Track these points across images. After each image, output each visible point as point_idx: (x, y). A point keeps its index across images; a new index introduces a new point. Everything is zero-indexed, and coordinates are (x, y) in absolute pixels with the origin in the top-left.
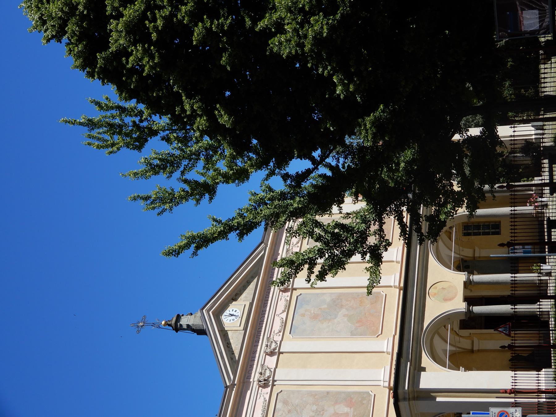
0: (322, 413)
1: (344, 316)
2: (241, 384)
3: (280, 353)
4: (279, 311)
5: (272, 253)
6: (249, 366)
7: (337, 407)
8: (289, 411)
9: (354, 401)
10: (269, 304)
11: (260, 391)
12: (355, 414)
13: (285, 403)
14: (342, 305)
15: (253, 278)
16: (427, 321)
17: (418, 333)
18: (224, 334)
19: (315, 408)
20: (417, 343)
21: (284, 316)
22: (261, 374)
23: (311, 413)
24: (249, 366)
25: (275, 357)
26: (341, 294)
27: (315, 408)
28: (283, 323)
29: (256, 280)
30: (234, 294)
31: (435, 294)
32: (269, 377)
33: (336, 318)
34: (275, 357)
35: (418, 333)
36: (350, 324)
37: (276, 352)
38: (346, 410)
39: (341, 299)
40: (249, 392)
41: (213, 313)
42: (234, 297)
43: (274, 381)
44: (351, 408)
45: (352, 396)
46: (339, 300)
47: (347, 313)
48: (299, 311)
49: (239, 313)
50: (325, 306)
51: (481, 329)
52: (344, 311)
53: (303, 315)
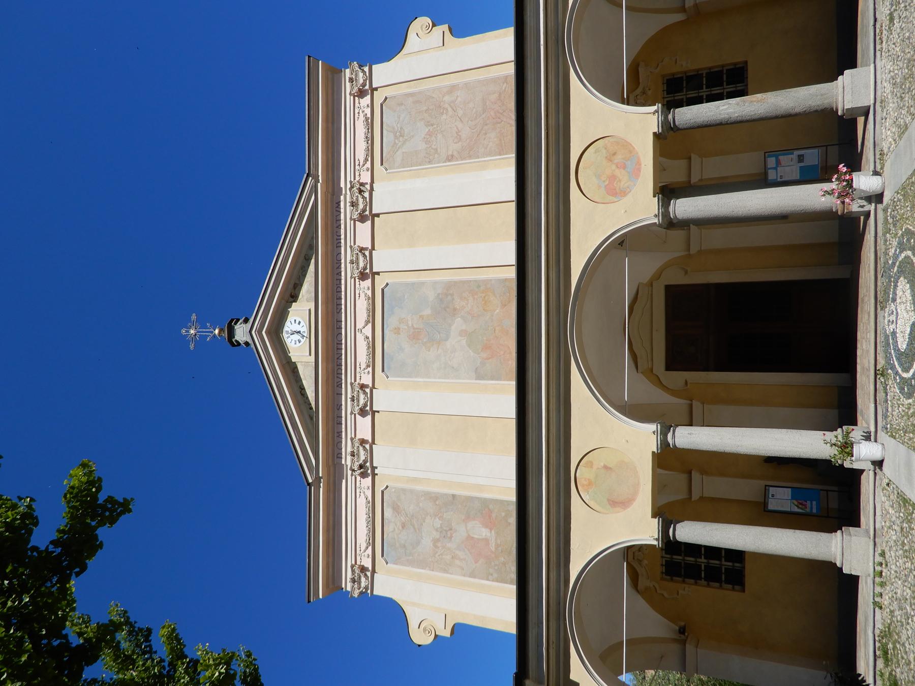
0: (449, 533)
1: (462, 333)
2: (332, 469)
3: (374, 90)
4: (359, 325)
5: (330, 190)
6: (336, 435)
7: (470, 524)
8: (404, 526)
9: (494, 515)
10: (343, 311)
11: (357, 286)
12: (499, 542)
13: (396, 509)
14: (455, 309)
15: (307, 260)
16: (575, 569)
17: (558, 591)
18: (291, 369)
19: (438, 523)
20: (558, 619)
21: (368, 331)
22: (353, 454)
23: (434, 533)
24: (336, 435)
25: (369, 223)
26: (450, 285)
27: (438, 523)
28: (369, 348)
29: (313, 261)
30: (291, 286)
31: (590, 484)
32: (365, 461)
33: (447, 340)
34: (369, 223)
35: (558, 591)
36: (472, 354)
37: (367, 90)
38: (484, 533)
39: (452, 295)
40: (344, 481)
41: (268, 333)
42: (292, 296)
43: (374, 468)
44: (491, 530)
45: (491, 507)
46: (449, 298)
47: (464, 327)
48: (391, 322)
49: (304, 329)
50: (427, 312)
51: (706, 369)
52: (458, 324)
53: (397, 331)
